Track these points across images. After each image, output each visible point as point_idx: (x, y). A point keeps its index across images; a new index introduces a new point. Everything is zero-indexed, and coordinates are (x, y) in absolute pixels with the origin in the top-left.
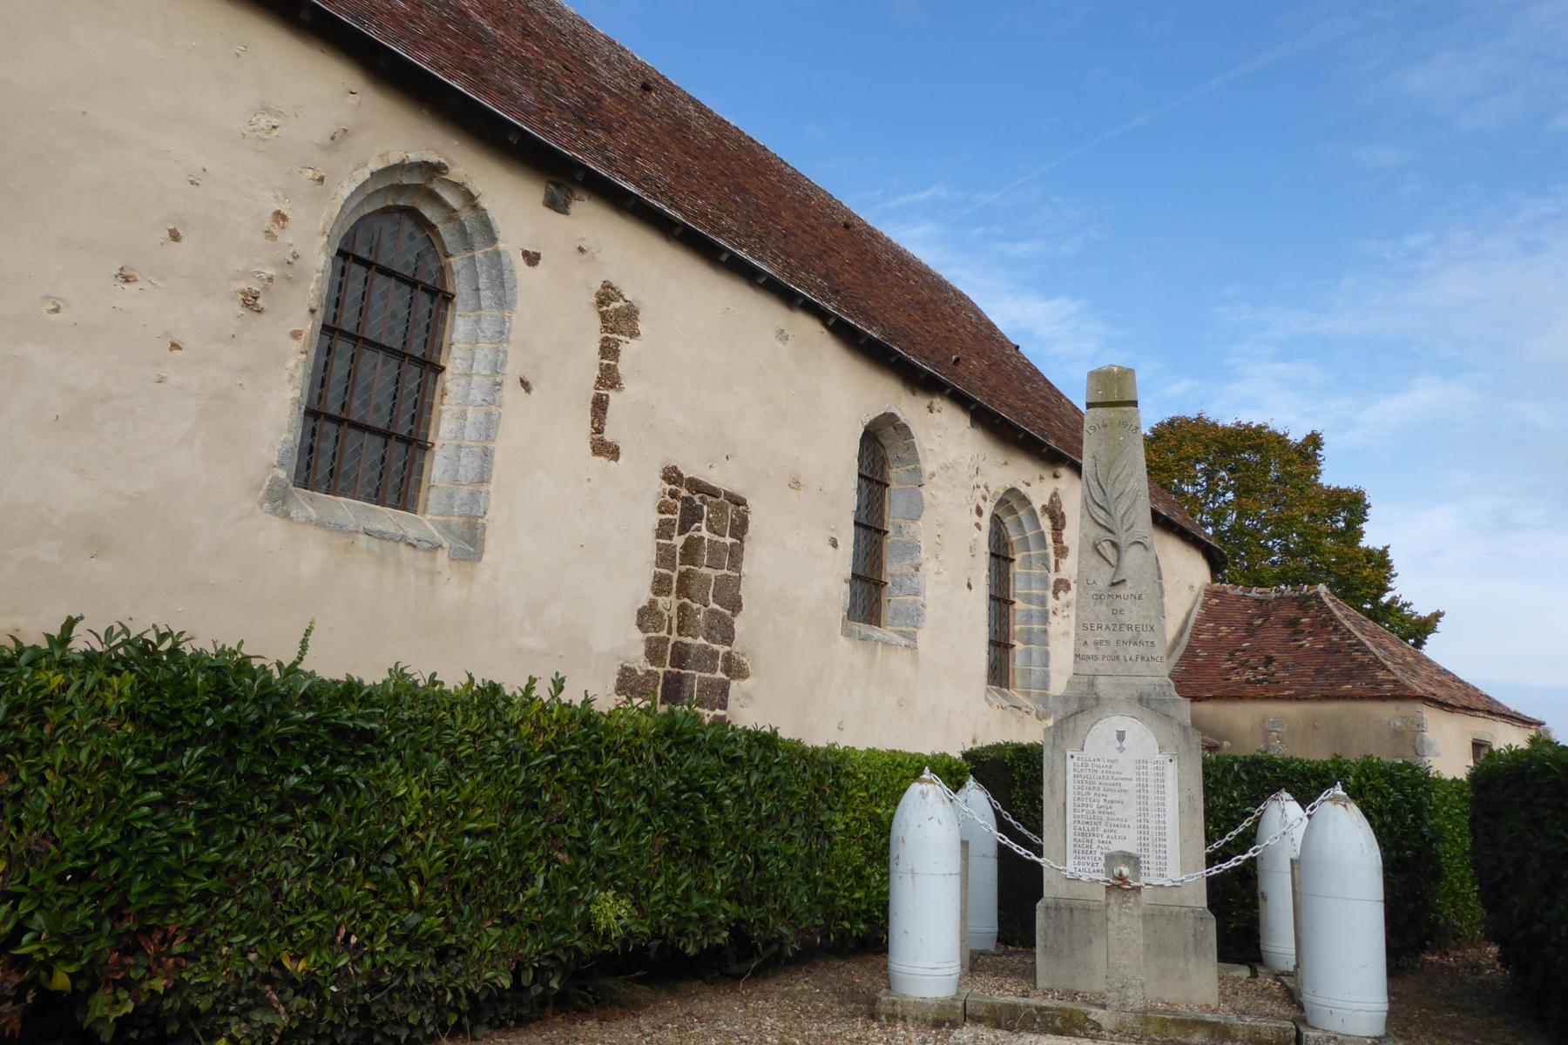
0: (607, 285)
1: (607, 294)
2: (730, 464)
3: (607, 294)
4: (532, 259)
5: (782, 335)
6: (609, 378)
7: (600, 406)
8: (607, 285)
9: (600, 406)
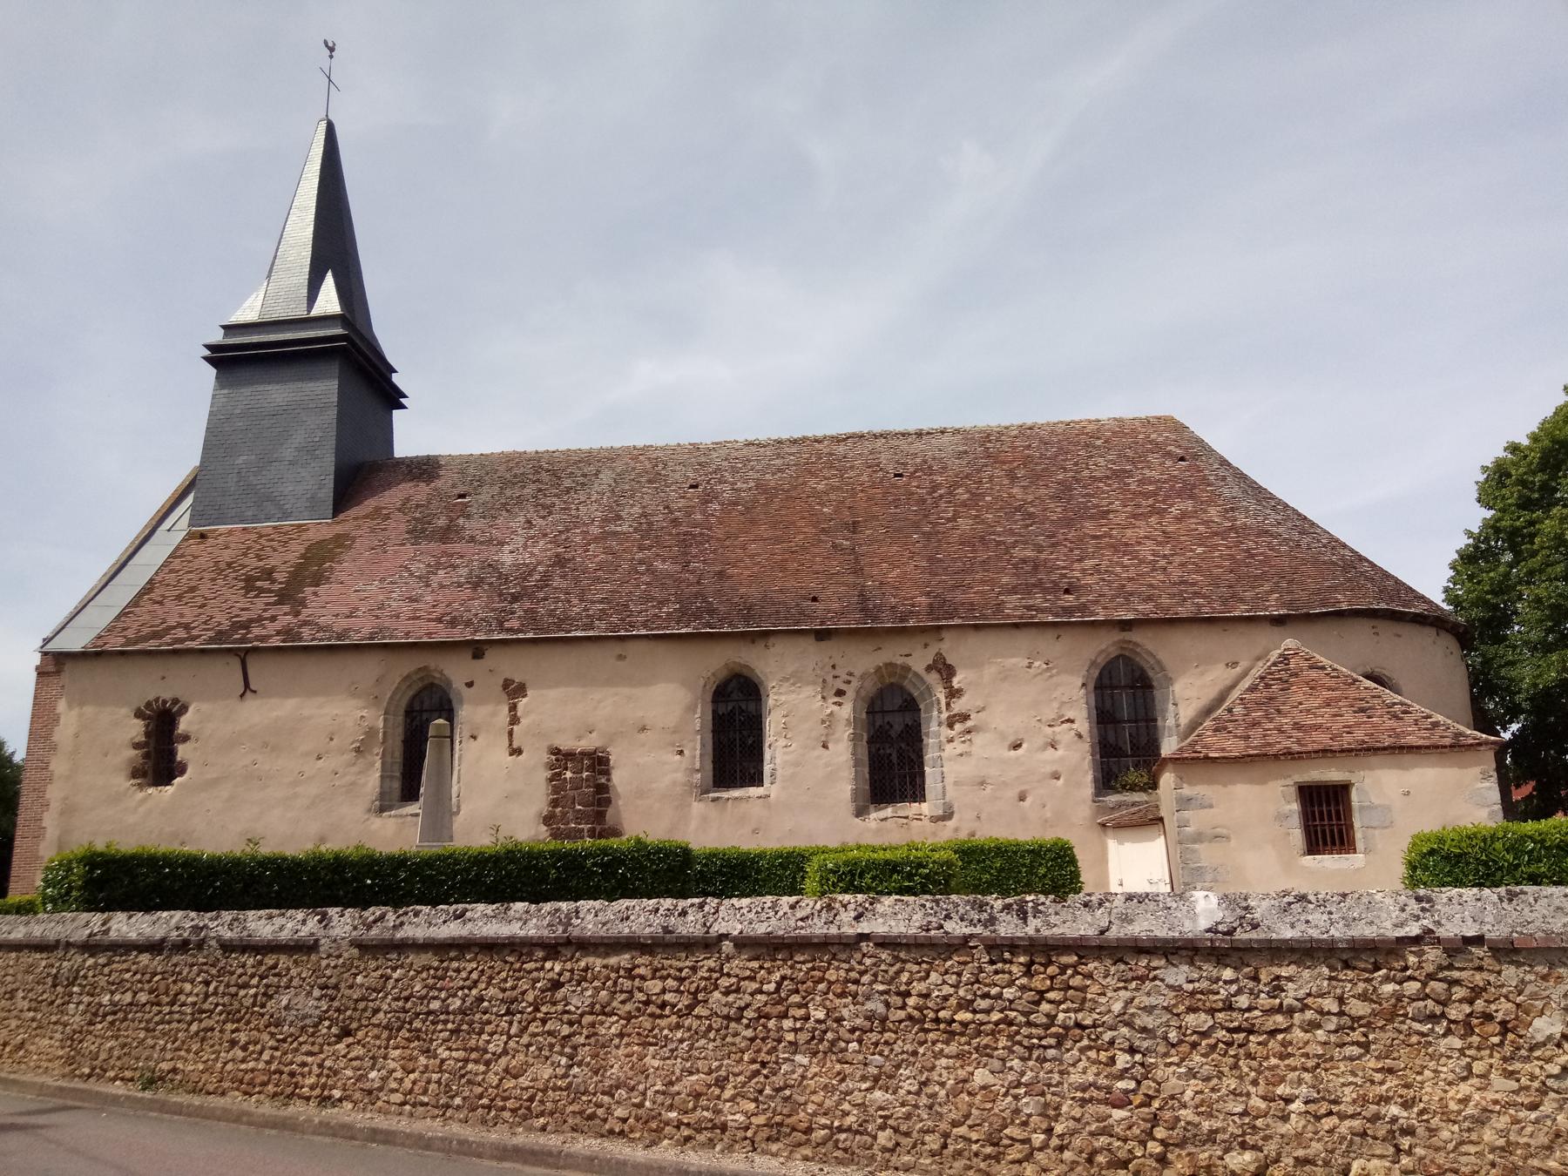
0: (506, 680)
1: (507, 684)
2: (594, 734)
3: (507, 684)
4: (470, 685)
5: (621, 657)
6: (514, 720)
7: (511, 733)
8: (506, 680)
9: (511, 733)
